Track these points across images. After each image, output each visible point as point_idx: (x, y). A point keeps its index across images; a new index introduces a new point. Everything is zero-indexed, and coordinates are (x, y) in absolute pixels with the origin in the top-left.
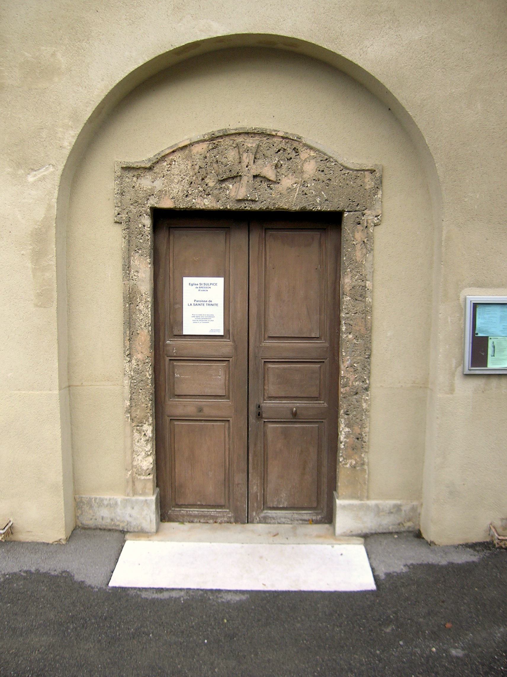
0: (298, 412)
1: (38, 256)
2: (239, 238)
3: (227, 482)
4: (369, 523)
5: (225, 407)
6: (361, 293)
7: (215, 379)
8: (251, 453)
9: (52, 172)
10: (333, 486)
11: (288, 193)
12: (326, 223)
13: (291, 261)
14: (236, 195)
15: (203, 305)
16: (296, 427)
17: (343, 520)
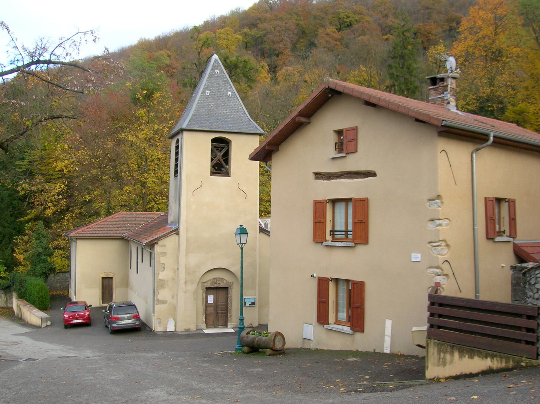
0: (91, 317)
1: (194, 294)
2: (215, 290)
3: (214, 323)
4: (232, 326)
5: (213, 312)
6: (231, 297)
7: (212, 309)
8: (217, 318)
9: (196, 284)
10: (227, 322)
11: (222, 285)
12: (226, 289)
13: (222, 293)
14: (216, 286)
15: (211, 299)
16: (520, 122)
17: (229, 326)
